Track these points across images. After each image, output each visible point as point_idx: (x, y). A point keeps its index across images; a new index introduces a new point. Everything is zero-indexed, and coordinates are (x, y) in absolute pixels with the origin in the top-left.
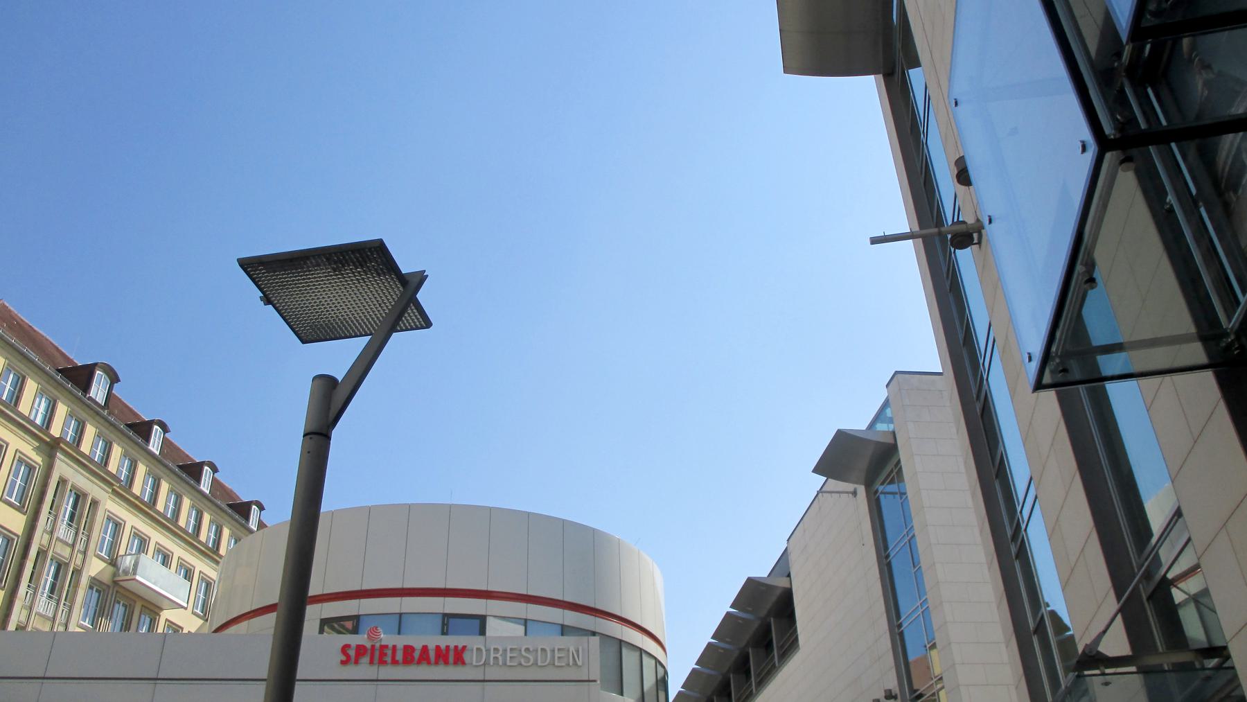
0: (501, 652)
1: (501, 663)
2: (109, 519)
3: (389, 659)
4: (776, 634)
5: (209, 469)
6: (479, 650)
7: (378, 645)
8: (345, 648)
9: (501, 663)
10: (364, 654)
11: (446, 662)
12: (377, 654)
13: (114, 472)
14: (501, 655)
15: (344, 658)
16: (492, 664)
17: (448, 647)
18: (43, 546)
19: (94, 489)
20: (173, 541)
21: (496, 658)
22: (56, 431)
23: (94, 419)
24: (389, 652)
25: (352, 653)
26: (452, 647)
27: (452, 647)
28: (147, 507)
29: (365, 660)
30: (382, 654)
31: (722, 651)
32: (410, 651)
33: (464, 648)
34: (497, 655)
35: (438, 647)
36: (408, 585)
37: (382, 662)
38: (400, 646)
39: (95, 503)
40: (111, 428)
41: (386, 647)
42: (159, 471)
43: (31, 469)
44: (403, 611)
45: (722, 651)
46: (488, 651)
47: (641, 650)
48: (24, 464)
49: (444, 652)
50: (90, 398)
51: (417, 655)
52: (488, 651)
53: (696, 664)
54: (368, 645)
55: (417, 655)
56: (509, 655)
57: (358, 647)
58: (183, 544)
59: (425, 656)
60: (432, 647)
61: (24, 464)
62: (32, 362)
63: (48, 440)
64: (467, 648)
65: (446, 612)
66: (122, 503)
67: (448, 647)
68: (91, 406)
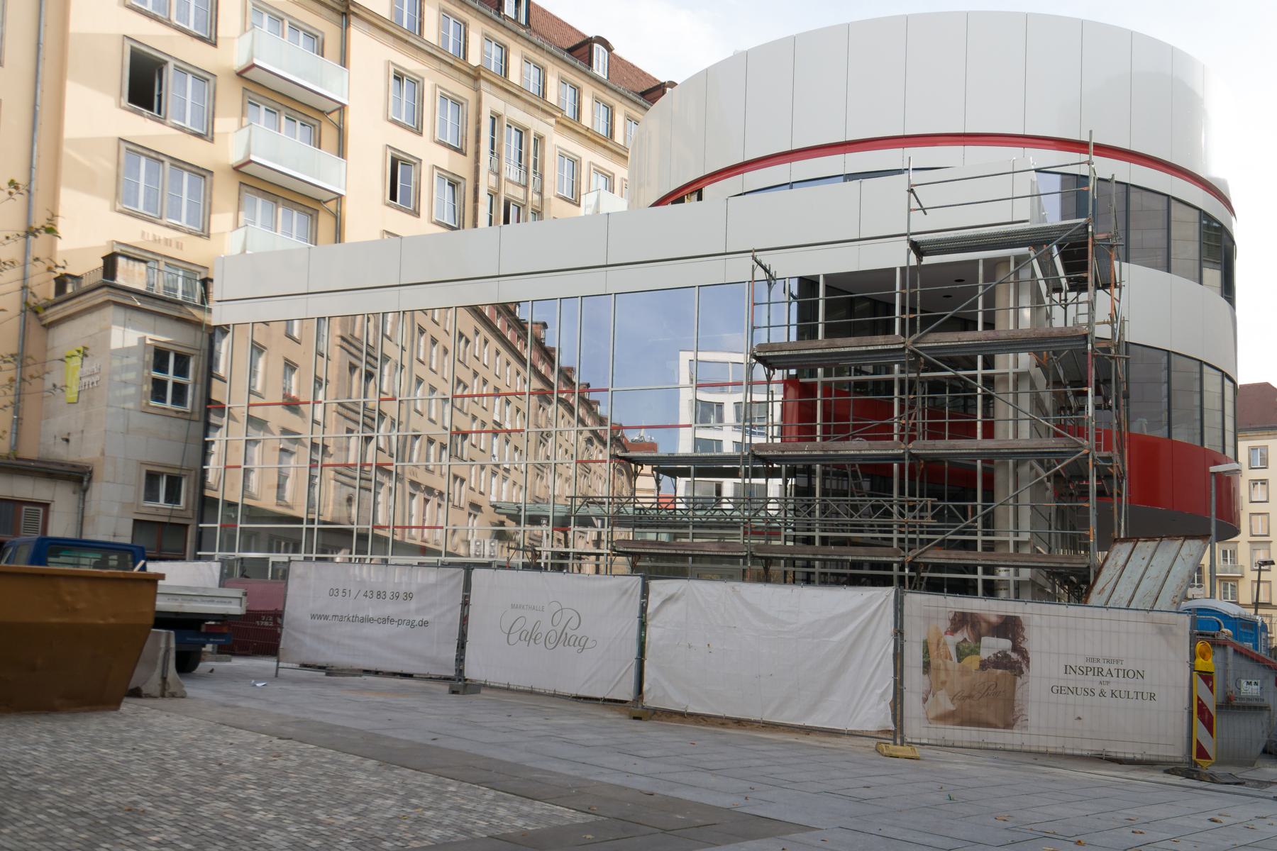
2: (561, 155)
13: (555, 103)
18: (492, 187)
19: (537, 124)
22: (474, 59)
39: (539, 139)
43: (457, 103)
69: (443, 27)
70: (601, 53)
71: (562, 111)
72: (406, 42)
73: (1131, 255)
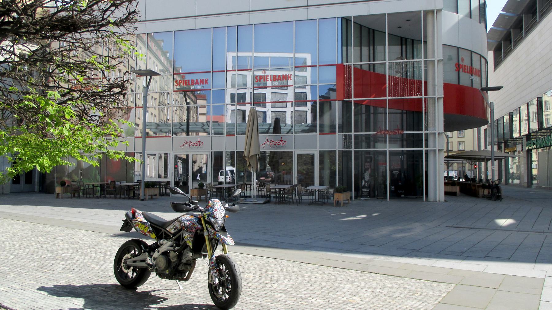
4: (539, 5)
8: (194, 81)
10: (262, 78)
12: (185, 81)
17: (463, 65)
25: (258, 78)
31: (507, 17)
33: (208, 79)
41: (187, 80)
45: (507, 17)
47: (480, 55)
51: (277, 78)
53: (502, 11)
55: (277, 78)
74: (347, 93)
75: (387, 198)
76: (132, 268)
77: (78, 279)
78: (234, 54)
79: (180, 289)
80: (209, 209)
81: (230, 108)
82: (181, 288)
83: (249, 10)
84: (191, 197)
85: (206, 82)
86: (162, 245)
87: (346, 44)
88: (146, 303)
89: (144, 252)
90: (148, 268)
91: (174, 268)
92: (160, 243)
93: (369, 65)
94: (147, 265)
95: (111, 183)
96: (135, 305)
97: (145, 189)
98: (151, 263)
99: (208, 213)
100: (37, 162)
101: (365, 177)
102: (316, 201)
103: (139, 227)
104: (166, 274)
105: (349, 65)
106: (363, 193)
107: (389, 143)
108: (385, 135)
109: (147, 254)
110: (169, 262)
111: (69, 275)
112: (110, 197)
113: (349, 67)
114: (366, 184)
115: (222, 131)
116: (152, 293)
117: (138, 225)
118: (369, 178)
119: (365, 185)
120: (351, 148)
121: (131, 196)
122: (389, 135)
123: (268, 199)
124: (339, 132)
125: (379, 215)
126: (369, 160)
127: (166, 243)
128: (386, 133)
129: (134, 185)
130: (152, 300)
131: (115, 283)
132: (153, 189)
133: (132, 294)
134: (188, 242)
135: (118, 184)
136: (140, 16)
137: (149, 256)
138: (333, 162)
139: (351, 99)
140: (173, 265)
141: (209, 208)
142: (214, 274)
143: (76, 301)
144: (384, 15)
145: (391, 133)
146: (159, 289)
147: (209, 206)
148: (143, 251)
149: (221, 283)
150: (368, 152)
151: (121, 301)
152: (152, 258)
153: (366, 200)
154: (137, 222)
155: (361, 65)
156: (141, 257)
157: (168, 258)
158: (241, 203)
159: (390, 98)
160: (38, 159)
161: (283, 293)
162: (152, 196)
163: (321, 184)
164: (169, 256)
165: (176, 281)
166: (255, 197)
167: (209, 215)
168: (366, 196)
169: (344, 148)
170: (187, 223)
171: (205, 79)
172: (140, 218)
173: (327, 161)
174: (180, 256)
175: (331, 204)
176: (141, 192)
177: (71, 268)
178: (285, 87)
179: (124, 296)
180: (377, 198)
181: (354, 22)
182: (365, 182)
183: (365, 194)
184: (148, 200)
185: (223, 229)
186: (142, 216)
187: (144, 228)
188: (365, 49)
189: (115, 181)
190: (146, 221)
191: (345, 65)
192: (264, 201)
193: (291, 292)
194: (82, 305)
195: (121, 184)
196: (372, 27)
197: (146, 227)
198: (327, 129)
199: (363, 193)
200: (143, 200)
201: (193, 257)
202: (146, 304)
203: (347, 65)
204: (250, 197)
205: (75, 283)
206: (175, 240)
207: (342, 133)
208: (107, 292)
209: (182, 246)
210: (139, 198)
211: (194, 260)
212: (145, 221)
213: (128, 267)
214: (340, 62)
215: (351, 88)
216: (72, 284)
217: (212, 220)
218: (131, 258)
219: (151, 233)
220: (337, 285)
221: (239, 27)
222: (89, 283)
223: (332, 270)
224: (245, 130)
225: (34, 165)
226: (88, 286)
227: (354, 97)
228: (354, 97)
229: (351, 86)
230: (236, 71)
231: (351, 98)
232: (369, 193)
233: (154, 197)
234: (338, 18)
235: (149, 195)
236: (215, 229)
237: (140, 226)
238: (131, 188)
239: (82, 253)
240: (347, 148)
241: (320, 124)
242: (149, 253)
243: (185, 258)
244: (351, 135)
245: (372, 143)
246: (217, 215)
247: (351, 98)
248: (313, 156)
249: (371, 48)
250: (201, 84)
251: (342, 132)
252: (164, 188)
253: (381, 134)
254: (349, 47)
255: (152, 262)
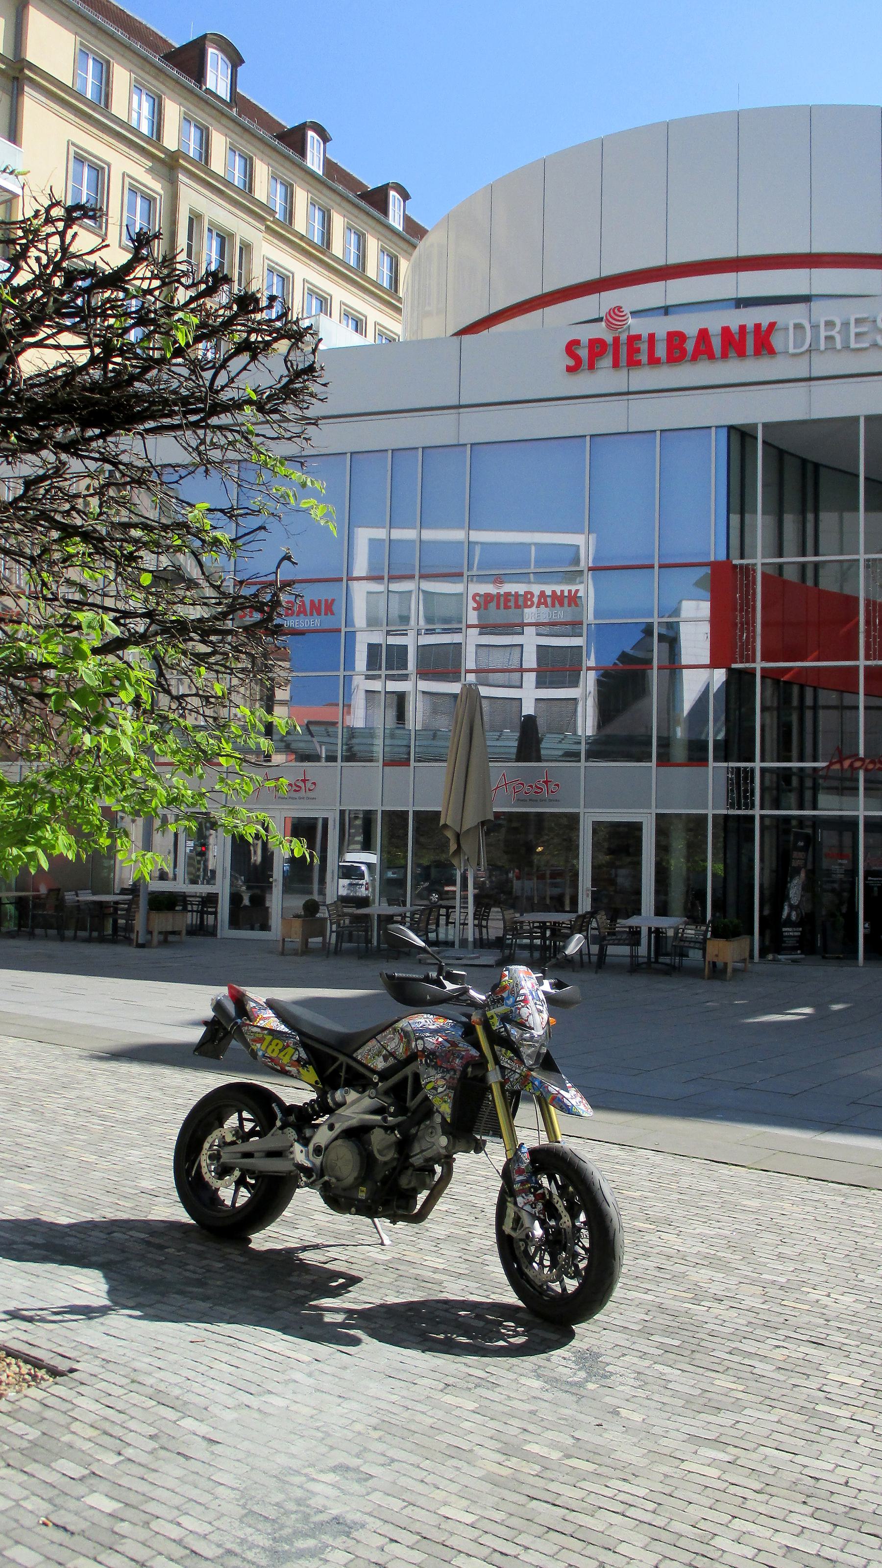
0: (838, 328)
1: (839, 346)
2: (271, 270)
3: (644, 357)
5: (397, 196)
6: (798, 327)
7: (624, 338)
9: (839, 346)
10: (602, 353)
11: (741, 353)
14: (838, 332)
15: (571, 363)
16: (822, 348)
20: (364, 300)
21: (829, 338)
22: (170, 142)
23: (219, 122)
24: (644, 347)
25: (583, 353)
26: (750, 327)
27: (750, 327)
28: (317, 251)
29: (606, 361)
30: (633, 350)
32: (676, 340)
33: (333, 600)
34: (833, 333)
35: (726, 331)
36: (673, 260)
37: (633, 363)
38: (661, 335)
39: (246, 248)
40: (247, 136)
41: (638, 337)
42: (327, 199)
43: (149, 200)
44: (669, 303)
46: (815, 327)
48: (139, 194)
49: (737, 337)
50: (208, 91)
51: (690, 346)
52: (815, 327)
54: (609, 338)
55: (690, 346)
56: (853, 330)
57: (592, 343)
58: (378, 304)
59: (703, 347)
60: (715, 330)
61: (139, 194)
62: (112, 36)
63: (163, 156)
64: (776, 327)
65: (740, 296)
66: (284, 247)
67: (743, 328)
68: (209, 100)
69: (309, 218)
70: (396, 200)
71: (272, 212)
72: (90, 117)
73: (873, 712)
74: (742, 645)
75: (857, 958)
76: (237, 1173)
77: (56, 1202)
78: (380, 534)
79: (382, 1244)
80: (502, 999)
81: (361, 684)
82: (387, 1241)
83: (456, 403)
84: (284, 940)
85: (329, 607)
86: (340, 1105)
87: (738, 508)
88: (301, 1292)
89: (282, 1128)
90: (297, 1177)
91: (385, 1180)
92: (333, 1099)
93: (803, 566)
94: (293, 1168)
95: (48, 895)
96: (267, 1298)
97: (148, 913)
98: (307, 1164)
99: (501, 1009)
100: (37, 843)
101: (791, 895)
102: (649, 962)
103: (264, 1048)
104: (360, 1200)
105: (748, 565)
106: (784, 942)
107: (865, 796)
108: (854, 770)
109: (291, 1134)
110: (367, 1161)
111: (22, 1185)
112: (46, 936)
113: (747, 571)
114: (794, 913)
115: (372, 752)
116: (302, 1256)
117: (261, 1040)
118: (802, 896)
119: (789, 915)
120: (753, 807)
121: (105, 933)
122: (867, 770)
123: (507, 952)
124: (716, 759)
125: (848, 1008)
126: (801, 844)
127: (354, 1102)
128: (858, 764)
129: (117, 903)
130: (314, 1282)
131: (173, 1218)
132: (170, 915)
133: (242, 1259)
134: (436, 1101)
135: (69, 896)
136: (325, 385)
137: (298, 1141)
138: (695, 848)
139: (752, 665)
140: (381, 1173)
141: (505, 995)
142: (528, 1208)
143: (78, 1278)
144: (855, 420)
145: (871, 766)
146: (318, 1241)
147: (504, 988)
148: (278, 1123)
149: (551, 1238)
150: (801, 820)
151: (219, 1283)
152: (311, 1147)
153: (794, 961)
154: (258, 1030)
155: (780, 566)
156: (272, 1141)
157: (366, 1150)
158: (429, 961)
159: (869, 663)
160: (39, 833)
161: (709, 1266)
162: (167, 934)
163: (662, 910)
164: (370, 1144)
165: (373, 1222)
166: (470, 946)
167: (505, 1019)
168: (793, 949)
169: (732, 806)
170: (432, 1040)
171: (326, 601)
172: (264, 1019)
173: (678, 845)
174: (404, 1146)
175: (695, 973)
176: (139, 923)
177: (19, 1160)
178: (516, 628)
179: (221, 1265)
180: (824, 958)
181: (764, 442)
182: (791, 907)
183: (790, 943)
184: (156, 947)
185: (547, 1064)
186: (269, 1013)
187: (281, 1051)
188: (790, 522)
189: (59, 890)
190: (286, 1030)
191: (735, 566)
192: (496, 958)
193: (734, 1265)
194: (105, 1295)
195: (80, 898)
196: (812, 457)
197: (288, 1046)
198: (679, 753)
199: (784, 942)
200: (142, 946)
201: (450, 1148)
202: (305, 1296)
203: (741, 566)
204: (450, 944)
205: (53, 1214)
206: (386, 1093)
207: (725, 764)
208: (161, 1247)
209: (414, 1113)
210: (133, 940)
211: (448, 1162)
212: (283, 1028)
213: (223, 1171)
214: (722, 557)
215: (754, 631)
216: (44, 1218)
217: (515, 1032)
218: (233, 1143)
219: (304, 1066)
220: (863, 1242)
221: (397, 454)
222: (95, 1216)
223: (816, 1189)
224: (404, 749)
225: (29, 849)
226: (91, 1226)
227: (764, 659)
228: (764, 659)
229: (754, 627)
230: (417, 577)
231: (754, 661)
232: (801, 939)
233: (171, 938)
234: (717, 427)
235: (160, 933)
236: (522, 1061)
237: (266, 1043)
238: (107, 911)
239: (34, 1111)
240: (739, 808)
241: (659, 738)
242: (299, 1131)
243: (422, 1151)
244: (752, 770)
245: (808, 795)
246: (531, 1017)
247: (754, 661)
248: (636, 828)
249: (810, 517)
250: (315, 613)
251: (726, 761)
252: (197, 912)
253: (842, 769)
254: (747, 516)
255: (308, 1160)
